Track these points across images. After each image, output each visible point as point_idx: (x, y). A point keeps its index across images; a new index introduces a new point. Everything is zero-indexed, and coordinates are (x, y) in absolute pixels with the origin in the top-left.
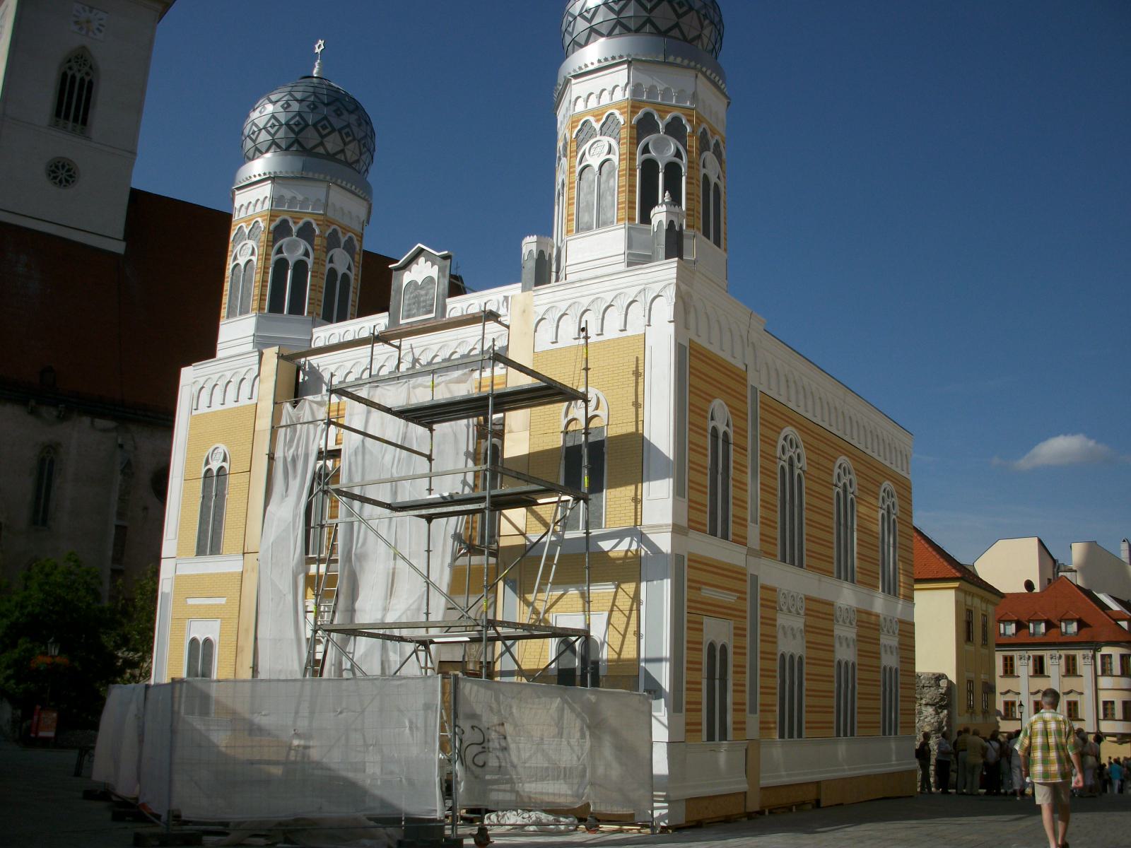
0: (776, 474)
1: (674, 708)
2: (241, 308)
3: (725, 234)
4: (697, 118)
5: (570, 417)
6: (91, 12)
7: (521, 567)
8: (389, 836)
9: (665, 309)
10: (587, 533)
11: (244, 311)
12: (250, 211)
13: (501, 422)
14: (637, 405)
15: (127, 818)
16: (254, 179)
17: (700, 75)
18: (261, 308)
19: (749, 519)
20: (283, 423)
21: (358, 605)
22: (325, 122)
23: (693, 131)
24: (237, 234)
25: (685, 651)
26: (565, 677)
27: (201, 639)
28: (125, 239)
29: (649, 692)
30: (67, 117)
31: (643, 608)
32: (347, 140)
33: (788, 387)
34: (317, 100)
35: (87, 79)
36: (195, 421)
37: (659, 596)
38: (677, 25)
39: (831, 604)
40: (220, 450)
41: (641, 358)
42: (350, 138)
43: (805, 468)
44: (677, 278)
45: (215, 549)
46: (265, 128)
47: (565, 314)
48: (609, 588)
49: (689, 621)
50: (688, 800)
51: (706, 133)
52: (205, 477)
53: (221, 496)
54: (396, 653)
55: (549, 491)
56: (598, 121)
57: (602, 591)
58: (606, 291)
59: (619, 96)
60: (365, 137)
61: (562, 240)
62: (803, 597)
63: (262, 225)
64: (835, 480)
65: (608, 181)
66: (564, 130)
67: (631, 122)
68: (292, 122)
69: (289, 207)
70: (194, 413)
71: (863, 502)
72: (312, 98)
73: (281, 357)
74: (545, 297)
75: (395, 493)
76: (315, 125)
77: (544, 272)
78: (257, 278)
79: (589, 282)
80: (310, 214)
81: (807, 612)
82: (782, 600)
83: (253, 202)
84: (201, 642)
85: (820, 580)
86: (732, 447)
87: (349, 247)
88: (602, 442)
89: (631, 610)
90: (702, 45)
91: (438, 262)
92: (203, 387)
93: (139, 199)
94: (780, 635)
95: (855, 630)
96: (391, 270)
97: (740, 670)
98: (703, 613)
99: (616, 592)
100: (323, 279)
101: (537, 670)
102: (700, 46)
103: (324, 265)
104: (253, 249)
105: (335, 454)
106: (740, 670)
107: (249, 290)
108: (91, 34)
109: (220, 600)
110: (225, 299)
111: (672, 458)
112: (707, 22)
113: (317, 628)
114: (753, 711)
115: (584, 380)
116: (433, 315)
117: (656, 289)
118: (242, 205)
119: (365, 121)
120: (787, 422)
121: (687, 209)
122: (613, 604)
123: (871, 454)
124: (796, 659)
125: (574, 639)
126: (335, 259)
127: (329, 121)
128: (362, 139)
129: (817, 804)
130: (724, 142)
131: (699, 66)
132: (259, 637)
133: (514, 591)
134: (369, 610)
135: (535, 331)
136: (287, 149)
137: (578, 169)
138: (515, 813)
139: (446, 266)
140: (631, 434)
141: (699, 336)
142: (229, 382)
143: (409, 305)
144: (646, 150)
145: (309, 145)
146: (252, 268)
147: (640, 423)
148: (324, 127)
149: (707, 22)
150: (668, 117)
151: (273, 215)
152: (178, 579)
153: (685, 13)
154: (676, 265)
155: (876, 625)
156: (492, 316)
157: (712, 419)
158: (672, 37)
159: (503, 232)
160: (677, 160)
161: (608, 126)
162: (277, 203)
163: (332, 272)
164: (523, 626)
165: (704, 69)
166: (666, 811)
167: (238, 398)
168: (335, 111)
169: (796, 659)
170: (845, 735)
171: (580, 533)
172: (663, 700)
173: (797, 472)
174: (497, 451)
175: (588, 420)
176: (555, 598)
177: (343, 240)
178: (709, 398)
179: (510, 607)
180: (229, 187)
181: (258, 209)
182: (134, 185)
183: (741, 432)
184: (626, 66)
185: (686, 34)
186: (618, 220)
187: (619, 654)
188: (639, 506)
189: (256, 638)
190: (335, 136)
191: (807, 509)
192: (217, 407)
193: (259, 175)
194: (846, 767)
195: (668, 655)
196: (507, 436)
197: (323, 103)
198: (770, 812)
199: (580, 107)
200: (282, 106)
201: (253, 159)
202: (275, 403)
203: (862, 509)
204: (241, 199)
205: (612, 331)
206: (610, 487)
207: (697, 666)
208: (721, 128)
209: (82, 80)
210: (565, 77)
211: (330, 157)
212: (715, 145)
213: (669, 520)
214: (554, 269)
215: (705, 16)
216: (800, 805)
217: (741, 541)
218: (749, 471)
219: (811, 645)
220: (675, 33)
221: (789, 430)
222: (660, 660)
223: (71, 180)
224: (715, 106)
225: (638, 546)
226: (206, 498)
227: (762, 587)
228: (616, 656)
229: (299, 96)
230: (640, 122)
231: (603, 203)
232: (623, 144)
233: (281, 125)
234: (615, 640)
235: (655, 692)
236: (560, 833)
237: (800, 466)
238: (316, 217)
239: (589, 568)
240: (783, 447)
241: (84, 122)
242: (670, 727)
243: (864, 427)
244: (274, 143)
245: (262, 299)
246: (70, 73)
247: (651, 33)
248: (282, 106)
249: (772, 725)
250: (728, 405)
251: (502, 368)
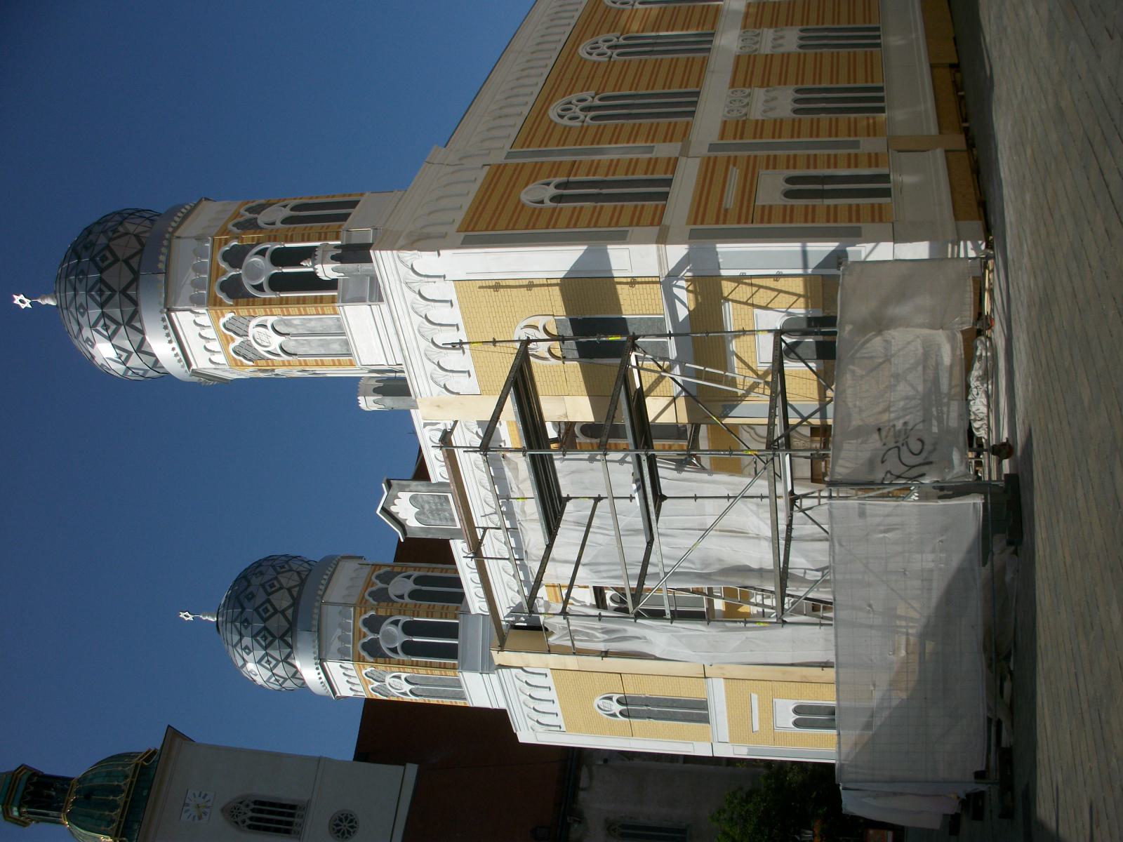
0: (625, 61)
1: (856, 235)
2: (455, 687)
3: (344, 196)
4: (222, 235)
5: (548, 355)
6: (188, 805)
7: (709, 402)
8: (1003, 551)
9: (426, 261)
10: (670, 335)
11: (458, 684)
12: (357, 681)
14: (530, 286)
15: (980, 803)
16: (324, 679)
17: (177, 234)
18: (454, 667)
19: (648, 156)
20: (569, 643)
21: (755, 566)
22: (260, 610)
23: (237, 238)
24: (380, 694)
25: (793, 225)
26: (826, 352)
27: (794, 717)
28: (404, 765)
29: (839, 264)
30: (290, 824)
31: (749, 272)
32: (277, 586)
33: (506, 116)
34: (239, 620)
35: (252, 806)
36: (572, 727)
37: (734, 255)
38: (127, 262)
39: (738, 58)
40: (601, 703)
41: (480, 283)
42: (276, 583)
43: (592, 93)
44: (392, 249)
45: (702, 705)
47: (438, 365)
48: (729, 310)
49: (762, 222)
50: (957, 217)
51: (239, 223)
52: (628, 716)
53: (647, 701)
54: (802, 528)
55: (625, 379)
56: (233, 340)
57: (732, 316)
58: (410, 324)
59: (205, 319)
60: (273, 567)
62: (731, 90)
63: (369, 669)
64: (604, 59)
65: (295, 326)
66: (247, 371)
67: (231, 305)
68: (263, 644)
69: (349, 643)
70: (564, 728)
71: (628, 26)
72: (238, 624)
73: (502, 648)
74: (420, 384)
75: (636, 532)
76: (265, 620)
77: (394, 386)
78: (423, 672)
79: (403, 342)
80: (354, 621)
81: (747, 85)
82: (735, 114)
83: (347, 678)
84: (798, 717)
85: (713, 72)
86: (572, 179)
87: (387, 578)
88: (572, 321)
89: (752, 285)
90: (145, 232)
91: (394, 493)
92: (538, 722)
93: (363, 754)
94: (772, 115)
95: (766, 30)
96: (406, 539)
97: (812, 161)
98: (752, 205)
99: (733, 301)
100: (420, 605)
101: (819, 384)
102: (147, 235)
103: (407, 604)
104: (394, 677)
105: (599, 592)
106: (812, 161)
107: (435, 680)
108: (209, 804)
109: (750, 702)
110: (447, 702)
111: (585, 247)
112: (121, 229)
113: (780, 621)
114: (855, 145)
115: (508, 344)
116: (450, 496)
117: (404, 271)
118: (351, 689)
119: (258, 567)
120: (574, 53)
121: (319, 240)
122: (746, 303)
123: (576, 18)
124: (798, 106)
125: (783, 345)
126: (399, 593)
127: (259, 607)
128: (275, 569)
129: (955, 67)
130: (248, 202)
131: (167, 236)
132: (790, 662)
133: (734, 407)
134: (761, 555)
135: (458, 394)
136: (291, 647)
137: (285, 357)
138: (972, 403)
139: (398, 484)
140: (561, 290)
141: (454, 220)
142: (530, 696)
143: (440, 519)
144: (259, 288)
145: (285, 625)
146: (413, 677)
147: (549, 282)
148: (266, 610)
149: (121, 229)
150: (224, 265)
151: (359, 659)
152: (734, 739)
153: (113, 254)
154: (378, 252)
155: (758, 8)
156: (445, 439)
157: (542, 202)
158: (139, 266)
159: (358, 429)
160: (268, 254)
161: (237, 329)
162: (345, 655)
163: (413, 595)
164: (772, 407)
165: (170, 230)
166: (969, 244)
167: (546, 687)
168: (249, 600)
169: (798, 106)
170: (879, 37)
171: (671, 343)
172: (848, 249)
173: (597, 102)
174: (587, 429)
175: (553, 338)
176: (741, 365)
177: (380, 585)
178: (520, 206)
179: (753, 411)
180: (334, 702)
181: (353, 673)
182: (351, 757)
183: (555, 168)
184: (173, 314)
185: (134, 251)
186: (336, 314)
187: (799, 296)
188: (639, 280)
189: (792, 665)
190: (273, 598)
191: (636, 89)
192: (556, 708)
193: (319, 674)
194: (914, 36)
195: (799, 244)
196: (571, 419)
197: (241, 613)
198: (965, 120)
199: (221, 358)
200: (248, 654)
201: (303, 679)
202: (549, 652)
203: (635, 27)
204: (344, 690)
205: (452, 315)
206: (620, 311)
207: (810, 210)
208: (233, 206)
209: (253, 810)
210: (191, 376)
211: (296, 602)
212: (250, 213)
213: (653, 248)
214: (393, 375)
215: (115, 231)
216: (958, 87)
217: (672, 164)
218: (597, 158)
219: (783, 81)
220: (134, 262)
221: (553, 114)
222: (805, 253)
223: (350, 818)
224: (210, 215)
225: (682, 279)
226: (650, 716)
227: (722, 138)
228: (802, 300)
229: (236, 638)
230: (230, 296)
231: (319, 330)
232: (254, 312)
233: (267, 654)
234: (785, 300)
235: (839, 258)
236: (995, 357)
237: (590, 99)
238: (357, 615)
239: (708, 333)
241: (293, 807)
242: (877, 240)
243: (547, 28)
244: (286, 660)
245: (444, 667)
246: (248, 822)
247: (137, 289)
248: (248, 654)
249: (871, 121)
250: (527, 185)
251: (500, 424)
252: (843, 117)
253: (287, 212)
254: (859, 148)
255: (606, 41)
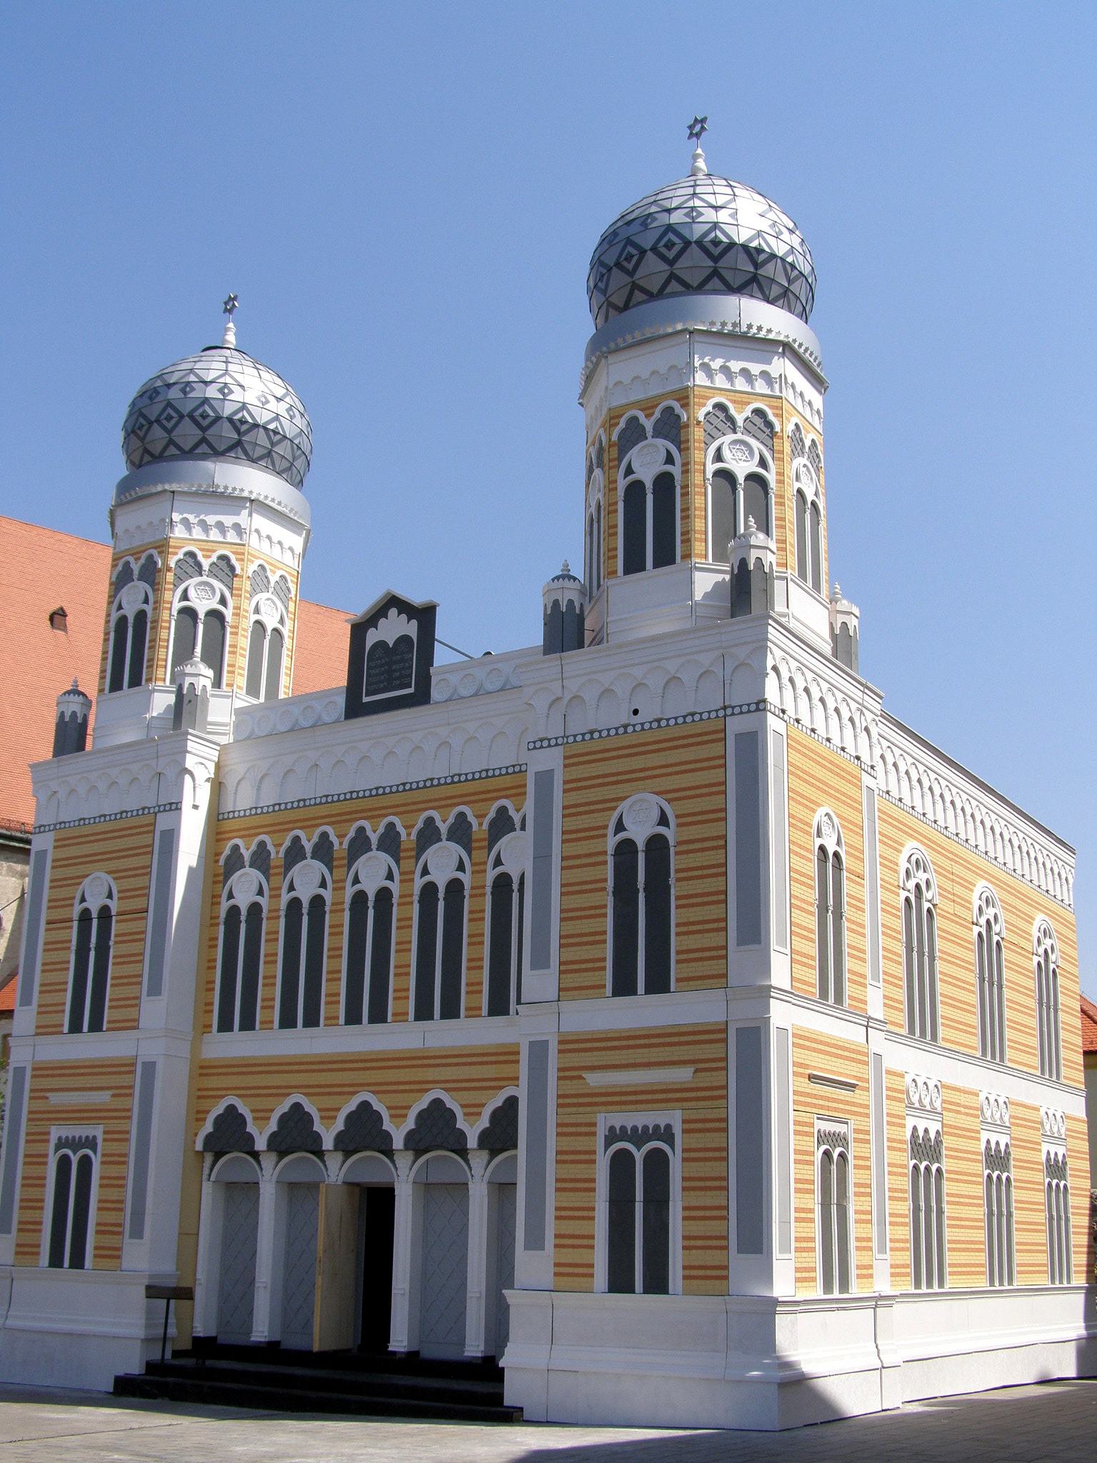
13: (723, 1027)
19: (869, 976)
25: (792, 1165)
46: (158, 421)
61: (599, 586)
86: (845, 874)
116: (411, 690)
148: (169, 418)
177: (274, 578)
178: (812, 805)
240: (907, 872)
252: (853, 1230)
253: (810, 497)
254: (131, 1237)
255: (928, 882)
